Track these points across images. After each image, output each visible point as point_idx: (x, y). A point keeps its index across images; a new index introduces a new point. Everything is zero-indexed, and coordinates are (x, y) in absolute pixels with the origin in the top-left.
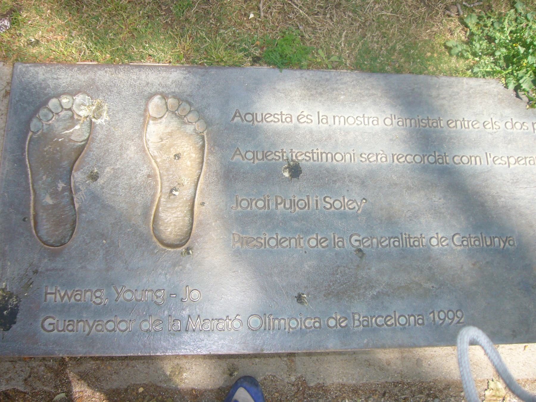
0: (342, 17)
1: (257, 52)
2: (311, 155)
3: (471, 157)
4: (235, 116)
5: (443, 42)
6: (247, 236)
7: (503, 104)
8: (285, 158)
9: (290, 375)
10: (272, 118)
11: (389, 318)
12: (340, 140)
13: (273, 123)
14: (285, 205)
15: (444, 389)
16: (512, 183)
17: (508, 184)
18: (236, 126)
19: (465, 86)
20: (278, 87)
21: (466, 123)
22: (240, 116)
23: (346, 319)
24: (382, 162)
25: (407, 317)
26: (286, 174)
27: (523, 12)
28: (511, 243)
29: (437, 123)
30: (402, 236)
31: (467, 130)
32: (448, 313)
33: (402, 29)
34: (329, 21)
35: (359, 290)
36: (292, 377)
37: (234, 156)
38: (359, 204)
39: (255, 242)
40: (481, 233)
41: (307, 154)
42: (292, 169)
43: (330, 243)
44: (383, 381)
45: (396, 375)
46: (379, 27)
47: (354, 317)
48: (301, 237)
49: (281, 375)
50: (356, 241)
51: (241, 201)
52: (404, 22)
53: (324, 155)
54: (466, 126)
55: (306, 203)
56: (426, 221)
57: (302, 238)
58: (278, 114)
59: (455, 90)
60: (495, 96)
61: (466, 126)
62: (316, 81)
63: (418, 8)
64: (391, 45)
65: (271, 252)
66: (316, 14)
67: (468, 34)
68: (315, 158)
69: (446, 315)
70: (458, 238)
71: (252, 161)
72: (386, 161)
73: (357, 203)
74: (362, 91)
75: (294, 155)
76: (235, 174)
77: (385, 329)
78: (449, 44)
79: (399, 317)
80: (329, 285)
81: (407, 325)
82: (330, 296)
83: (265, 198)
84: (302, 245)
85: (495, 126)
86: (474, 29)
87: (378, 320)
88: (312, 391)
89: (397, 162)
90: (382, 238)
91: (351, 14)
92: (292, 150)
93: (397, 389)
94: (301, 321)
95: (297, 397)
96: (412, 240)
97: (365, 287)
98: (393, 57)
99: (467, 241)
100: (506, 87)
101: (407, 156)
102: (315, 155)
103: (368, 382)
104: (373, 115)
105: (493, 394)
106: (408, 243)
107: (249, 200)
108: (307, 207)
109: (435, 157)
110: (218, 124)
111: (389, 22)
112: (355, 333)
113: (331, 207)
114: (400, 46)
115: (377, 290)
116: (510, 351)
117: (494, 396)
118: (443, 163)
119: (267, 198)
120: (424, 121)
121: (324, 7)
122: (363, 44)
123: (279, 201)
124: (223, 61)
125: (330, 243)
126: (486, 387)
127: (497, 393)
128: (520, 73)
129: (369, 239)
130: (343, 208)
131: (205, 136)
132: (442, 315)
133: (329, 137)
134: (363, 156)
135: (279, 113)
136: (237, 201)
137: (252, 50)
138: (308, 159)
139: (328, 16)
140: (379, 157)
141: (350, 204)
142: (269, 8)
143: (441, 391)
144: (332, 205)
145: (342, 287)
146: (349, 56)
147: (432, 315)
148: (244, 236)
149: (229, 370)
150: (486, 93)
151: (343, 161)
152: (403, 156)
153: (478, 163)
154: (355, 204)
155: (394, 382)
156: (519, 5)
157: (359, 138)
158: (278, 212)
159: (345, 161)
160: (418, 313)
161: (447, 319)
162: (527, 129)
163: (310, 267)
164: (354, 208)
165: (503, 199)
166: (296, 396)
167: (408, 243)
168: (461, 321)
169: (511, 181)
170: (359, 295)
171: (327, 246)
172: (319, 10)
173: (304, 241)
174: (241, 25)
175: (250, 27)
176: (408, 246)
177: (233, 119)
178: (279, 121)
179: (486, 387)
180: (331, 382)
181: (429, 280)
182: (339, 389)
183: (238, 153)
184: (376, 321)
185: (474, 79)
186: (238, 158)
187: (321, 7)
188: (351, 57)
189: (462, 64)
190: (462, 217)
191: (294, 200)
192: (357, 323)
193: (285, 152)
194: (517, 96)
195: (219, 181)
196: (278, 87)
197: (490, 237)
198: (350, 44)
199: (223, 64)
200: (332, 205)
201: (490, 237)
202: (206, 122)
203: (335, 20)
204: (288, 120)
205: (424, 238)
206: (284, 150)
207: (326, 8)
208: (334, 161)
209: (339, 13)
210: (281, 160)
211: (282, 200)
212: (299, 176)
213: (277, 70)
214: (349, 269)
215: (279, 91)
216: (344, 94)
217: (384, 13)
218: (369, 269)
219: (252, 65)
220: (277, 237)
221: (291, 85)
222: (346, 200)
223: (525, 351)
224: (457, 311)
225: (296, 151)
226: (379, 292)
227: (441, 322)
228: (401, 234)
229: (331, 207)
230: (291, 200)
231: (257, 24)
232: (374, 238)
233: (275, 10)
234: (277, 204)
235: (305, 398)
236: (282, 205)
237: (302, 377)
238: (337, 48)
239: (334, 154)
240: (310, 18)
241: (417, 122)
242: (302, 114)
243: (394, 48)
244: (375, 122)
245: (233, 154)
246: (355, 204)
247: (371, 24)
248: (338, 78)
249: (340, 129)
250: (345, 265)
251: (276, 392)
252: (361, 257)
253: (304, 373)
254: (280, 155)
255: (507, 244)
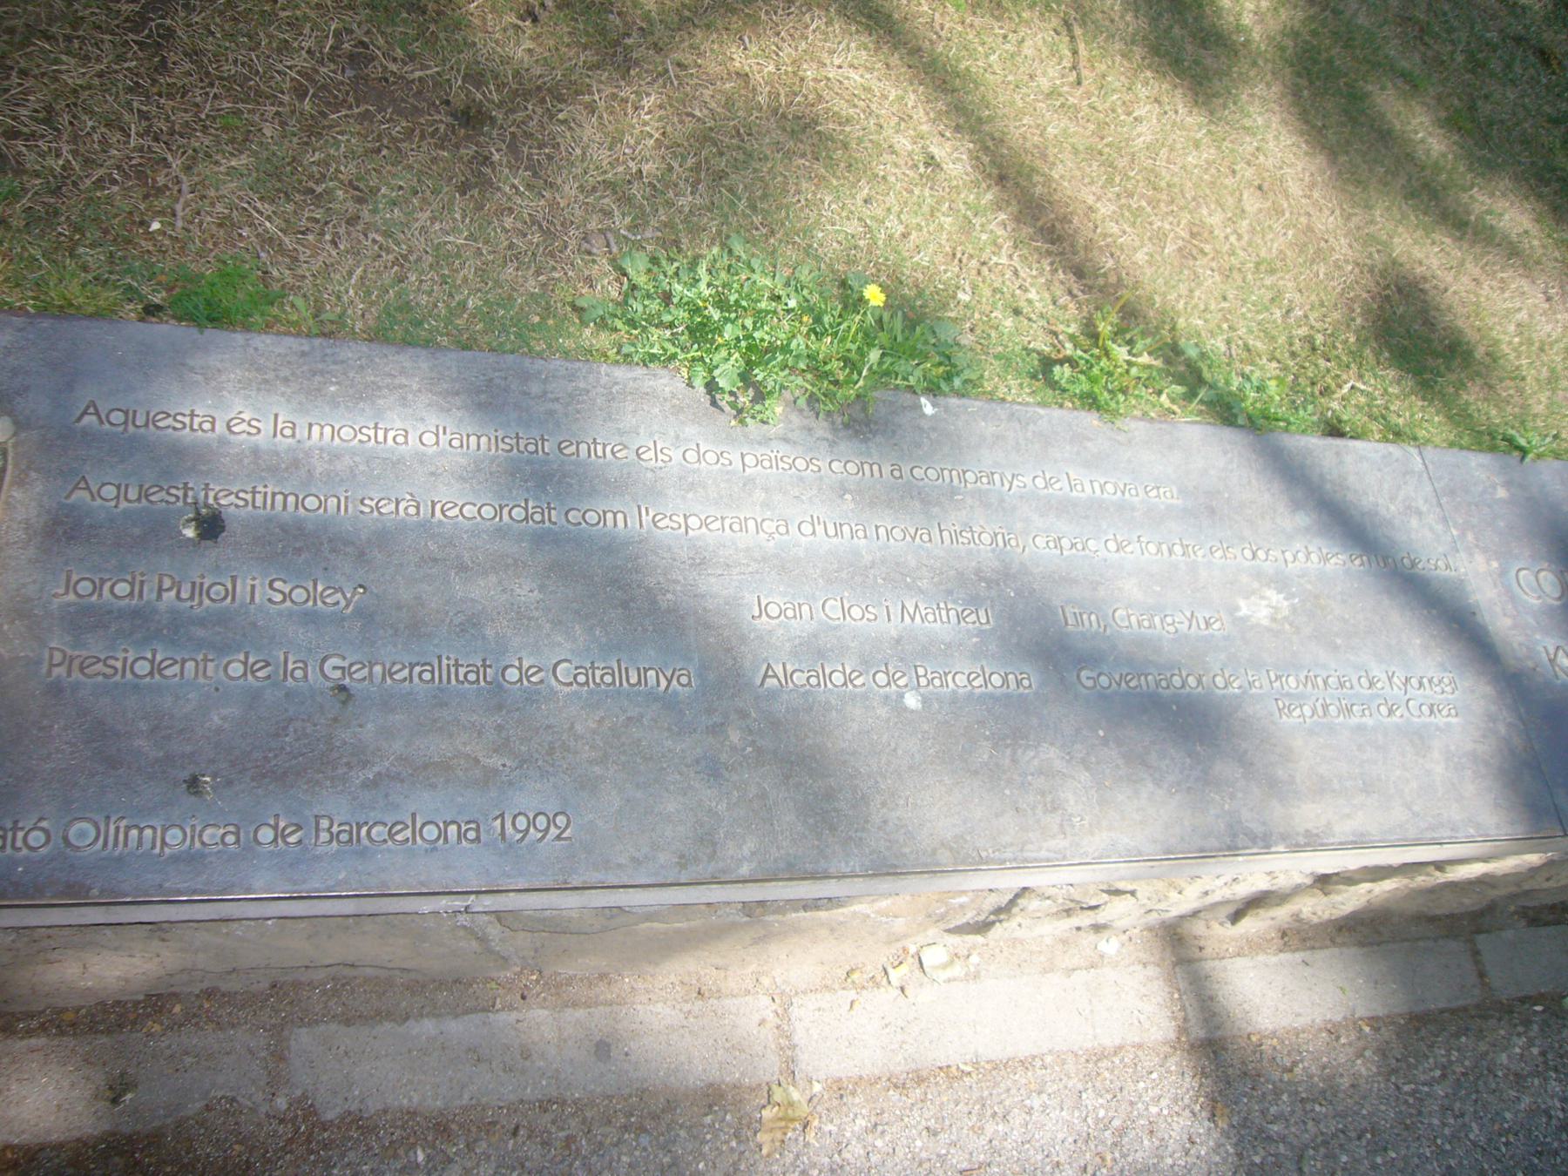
0: (359, 242)
1: (159, 296)
2: (249, 497)
3: (605, 513)
4: (85, 413)
5: (569, 299)
6: (85, 653)
7: (681, 417)
8: (189, 500)
9: (273, 1095)
10: (170, 421)
11: (399, 827)
12: (319, 470)
13: (170, 430)
14: (178, 592)
15: (663, 1111)
16: (691, 565)
17: (682, 566)
18: (85, 433)
19: (604, 380)
20: (191, 362)
21: (599, 448)
22: (97, 413)
23: (299, 828)
24: (407, 514)
25: (441, 825)
26: (190, 533)
27: (744, 256)
28: (684, 680)
29: (536, 445)
30: (440, 662)
31: (601, 460)
32: (534, 818)
33: (484, 271)
34: (328, 247)
35: (334, 769)
36: (279, 1100)
37: (72, 492)
38: (349, 595)
39: (99, 666)
40: (618, 661)
41: (242, 495)
42: (205, 522)
43: (276, 672)
44: (512, 1097)
45: (544, 1083)
46: (438, 263)
47: (317, 824)
48: (210, 657)
49: (251, 1095)
50: (335, 668)
51: (77, 582)
52: (490, 258)
53: (279, 498)
54: (600, 453)
55: (227, 590)
56: (497, 633)
57: (212, 660)
58: (184, 415)
59: (582, 385)
60: (665, 400)
61: (600, 453)
62: (279, 355)
63: (525, 235)
64: (457, 299)
65: (136, 686)
66: (303, 233)
67: (625, 287)
68: (259, 502)
69: (532, 823)
70: (568, 670)
71: (113, 503)
72: (418, 513)
73: (343, 594)
74: (378, 379)
75: (211, 494)
76: (71, 529)
77: (389, 850)
78: (581, 303)
79: (424, 825)
80: (265, 758)
81: (441, 841)
82: (267, 780)
83: (134, 578)
84: (210, 673)
85: (660, 456)
86: (641, 280)
87: (374, 831)
88: (332, 1132)
89: (442, 517)
90: (394, 664)
91: (379, 238)
92: (207, 485)
93: (548, 1117)
94: (193, 830)
95: (291, 1152)
96: (462, 671)
97: (348, 764)
98: (458, 322)
99: (587, 675)
100: (690, 385)
101: (463, 506)
102: (259, 498)
103: (474, 1102)
104: (398, 424)
105: (781, 1115)
106: (453, 677)
107: (97, 581)
108: (230, 598)
109: (526, 509)
110: (42, 427)
111: (458, 255)
112: (318, 858)
113: (284, 601)
114: (477, 301)
115: (376, 769)
116: (817, 1013)
117: (780, 1119)
118: (543, 521)
119: (139, 578)
120: (507, 440)
121: (322, 221)
122: (399, 295)
123: (167, 583)
124: (73, 305)
125: (276, 672)
126: (764, 1101)
127: (790, 1112)
128: (717, 358)
129: (364, 666)
130: (311, 603)
131: (10, 450)
132: (522, 823)
133: (296, 464)
134: (366, 502)
135: (188, 412)
136: (68, 580)
137: (145, 290)
138: (241, 503)
139: (328, 237)
140: (402, 506)
141: (329, 595)
142: (198, 213)
143: (655, 1117)
144: (286, 597)
145: (294, 762)
146: (363, 315)
147: (499, 821)
148: (77, 653)
149: (111, 1088)
150: (647, 394)
151: (322, 510)
152: (456, 505)
153: (621, 524)
154: (339, 595)
155: (541, 1101)
156: (736, 243)
157: (362, 468)
158: (162, 606)
159: (325, 510)
160: (468, 819)
161: (532, 830)
162: (731, 463)
163: (224, 719)
164: (338, 603)
165: (669, 596)
166: (288, 1148)
167: (453, 677)
168: (564, 835)
169: (690, 561)
170: (332, 779)
171: (268, 677)
172: (309, 225)
173: (217, 667)
174: (129, 242)
175: (150, 248)
176: (453, 681)
177: (79, 419)
178: (184, 427)
179: (764, 1101)
180: (380, 1106)
181: (495, 751)
182: (400, 1123)
183: (82, 485)
184: (369, 832)
185: (623, 368)
186: (81, 495)
187: (317, 221)
188: (367, 316)
189: (604, 340)
190: (577, 627)
191: (202, 584)
192: (324, 836)
193: (192, 489)
194: (714, 403)
195: (30, 540)
196: (191, 362)
197: (638, 669)
198: (368, 293)
199: (73, 311)
200: (286, 597)
201: (638, 669)
202: (16, 423)
203: (342, 247)
204: (207, 426)
205: (490, 666)
206: (190, 485)
207: (326, 223)
208: (301, 510)
209: (354, 235)
210: (180, 504)
211: (173, 583)
212: (217, 537)
213: (194, 331)
214: (315, 725)
215: (192, 369)
216: (337, 383)
217: (451, 239)
218: (361, 726)
219: (141, 320)
220: (154, 656)
221: (222, 361)
222: (320, 588)
223: (852, 1012)
224: (556, 815)
225: (218, 488)
226: (379, 774)
227: (519, 836)
228: (440, 658)
229: (284, 601)
230: (194, 584)
231: (167, 242)
232: (376, 663)
233: (209, 219)
234: (160, 590)
235: (312, 1152)
236: (173, 593)
237: (307, 1098)
238: (339, 298)
239: (301, 498)
240: (286, 240)
241: (493, 441)
242: (241, 416)
243: (463, 305)
244: (400, 439)
245: (70, 487)
246: (339, 595)
247: (419, 259)
248: (328, 351)
249: (321, 449)
250: (305, 717)
251: (237, 1142)
252: (344, 703)
253: (310, 1088)
254: (180, 493)
255: (674, 682)
